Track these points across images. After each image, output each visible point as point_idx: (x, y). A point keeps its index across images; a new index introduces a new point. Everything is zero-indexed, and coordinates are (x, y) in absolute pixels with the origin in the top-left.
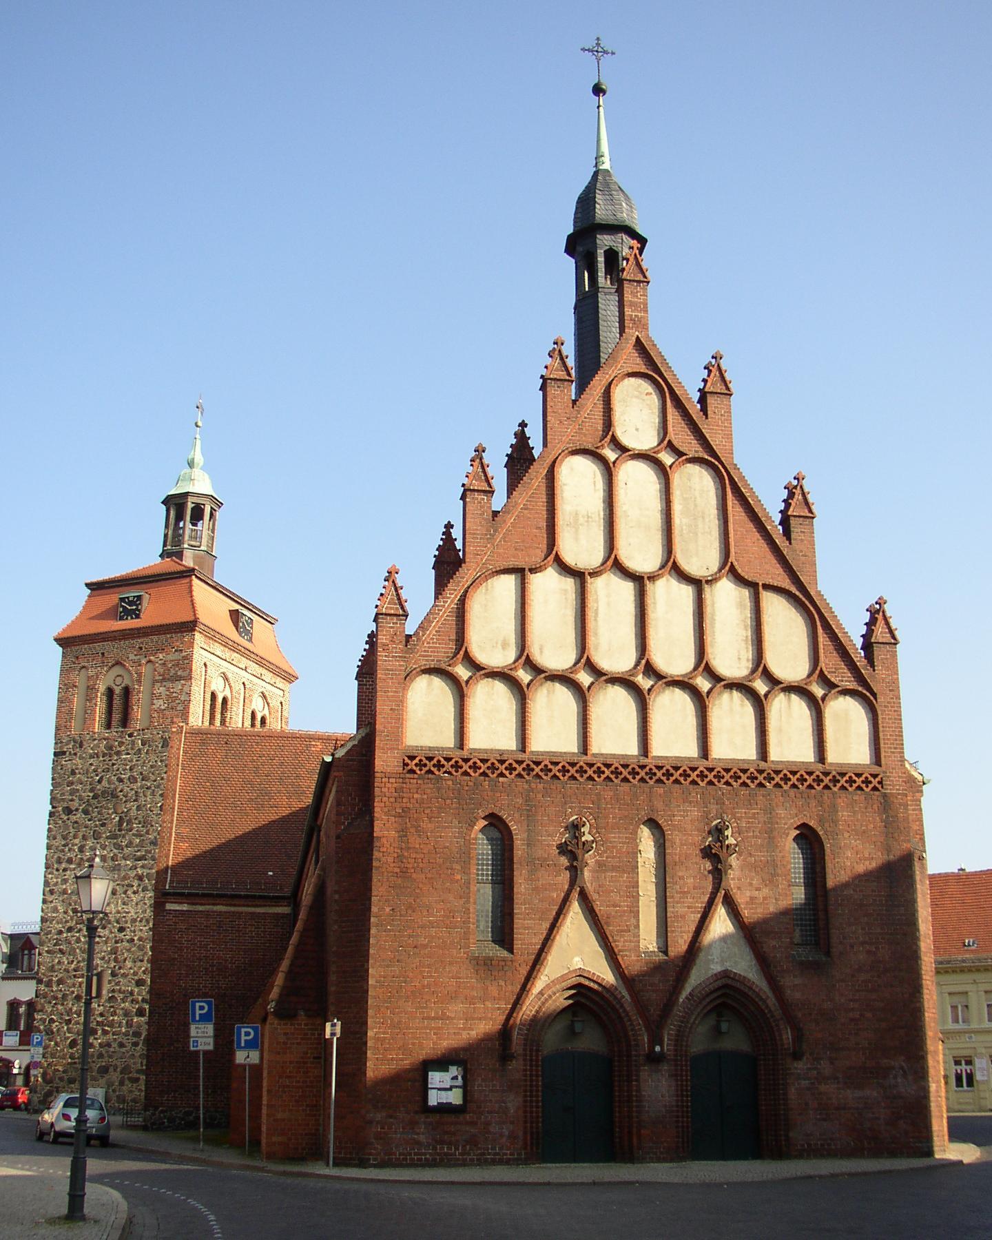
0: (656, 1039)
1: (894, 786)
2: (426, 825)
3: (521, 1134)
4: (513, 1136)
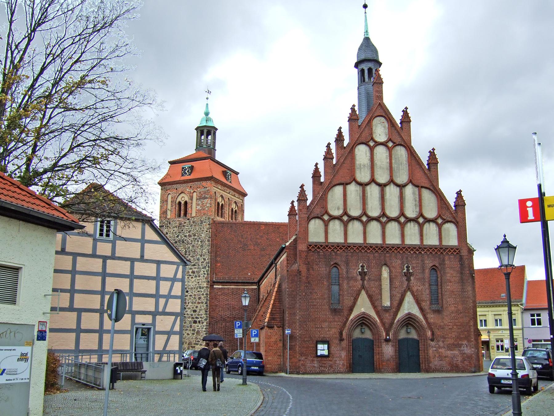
0: (387, 334)
1: (464, 253)
2: (315, 267)
3: (346, 364)
4: (343, 365)
